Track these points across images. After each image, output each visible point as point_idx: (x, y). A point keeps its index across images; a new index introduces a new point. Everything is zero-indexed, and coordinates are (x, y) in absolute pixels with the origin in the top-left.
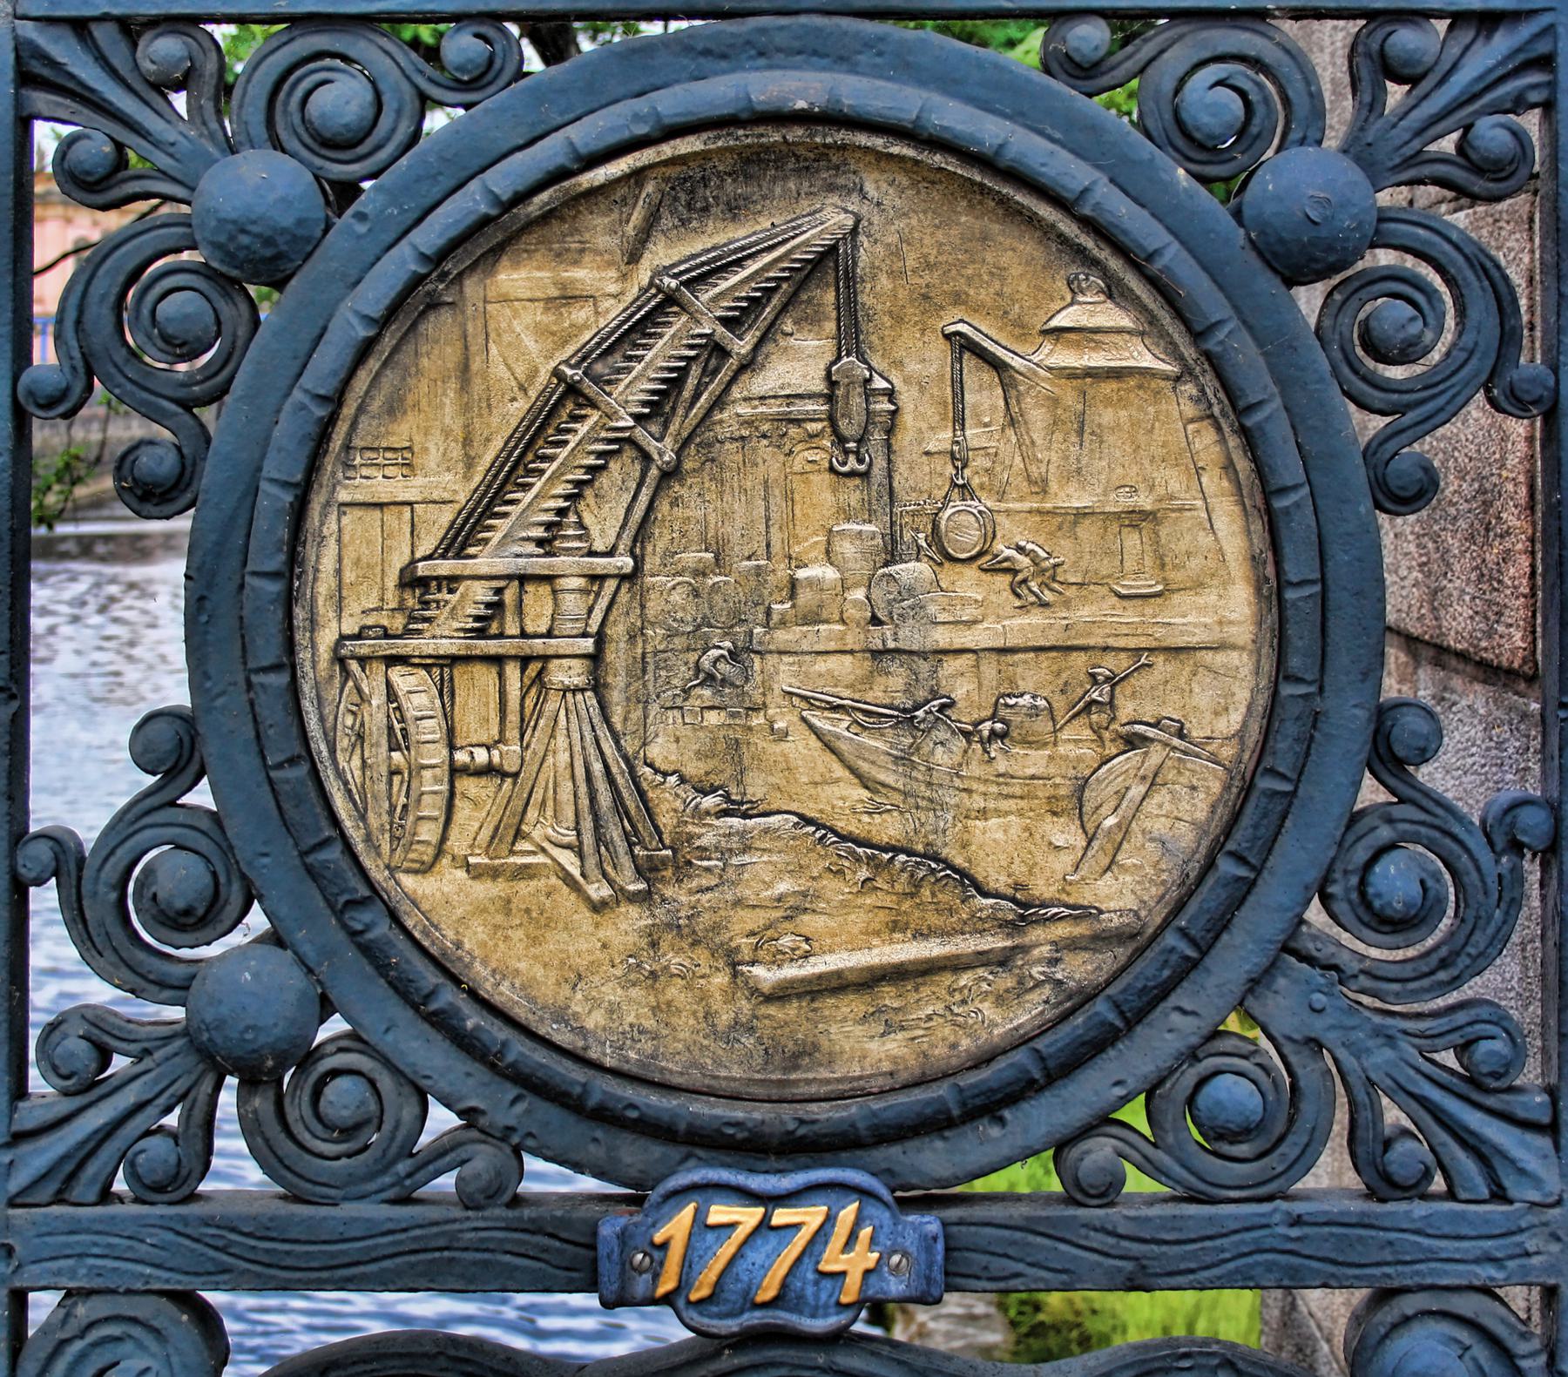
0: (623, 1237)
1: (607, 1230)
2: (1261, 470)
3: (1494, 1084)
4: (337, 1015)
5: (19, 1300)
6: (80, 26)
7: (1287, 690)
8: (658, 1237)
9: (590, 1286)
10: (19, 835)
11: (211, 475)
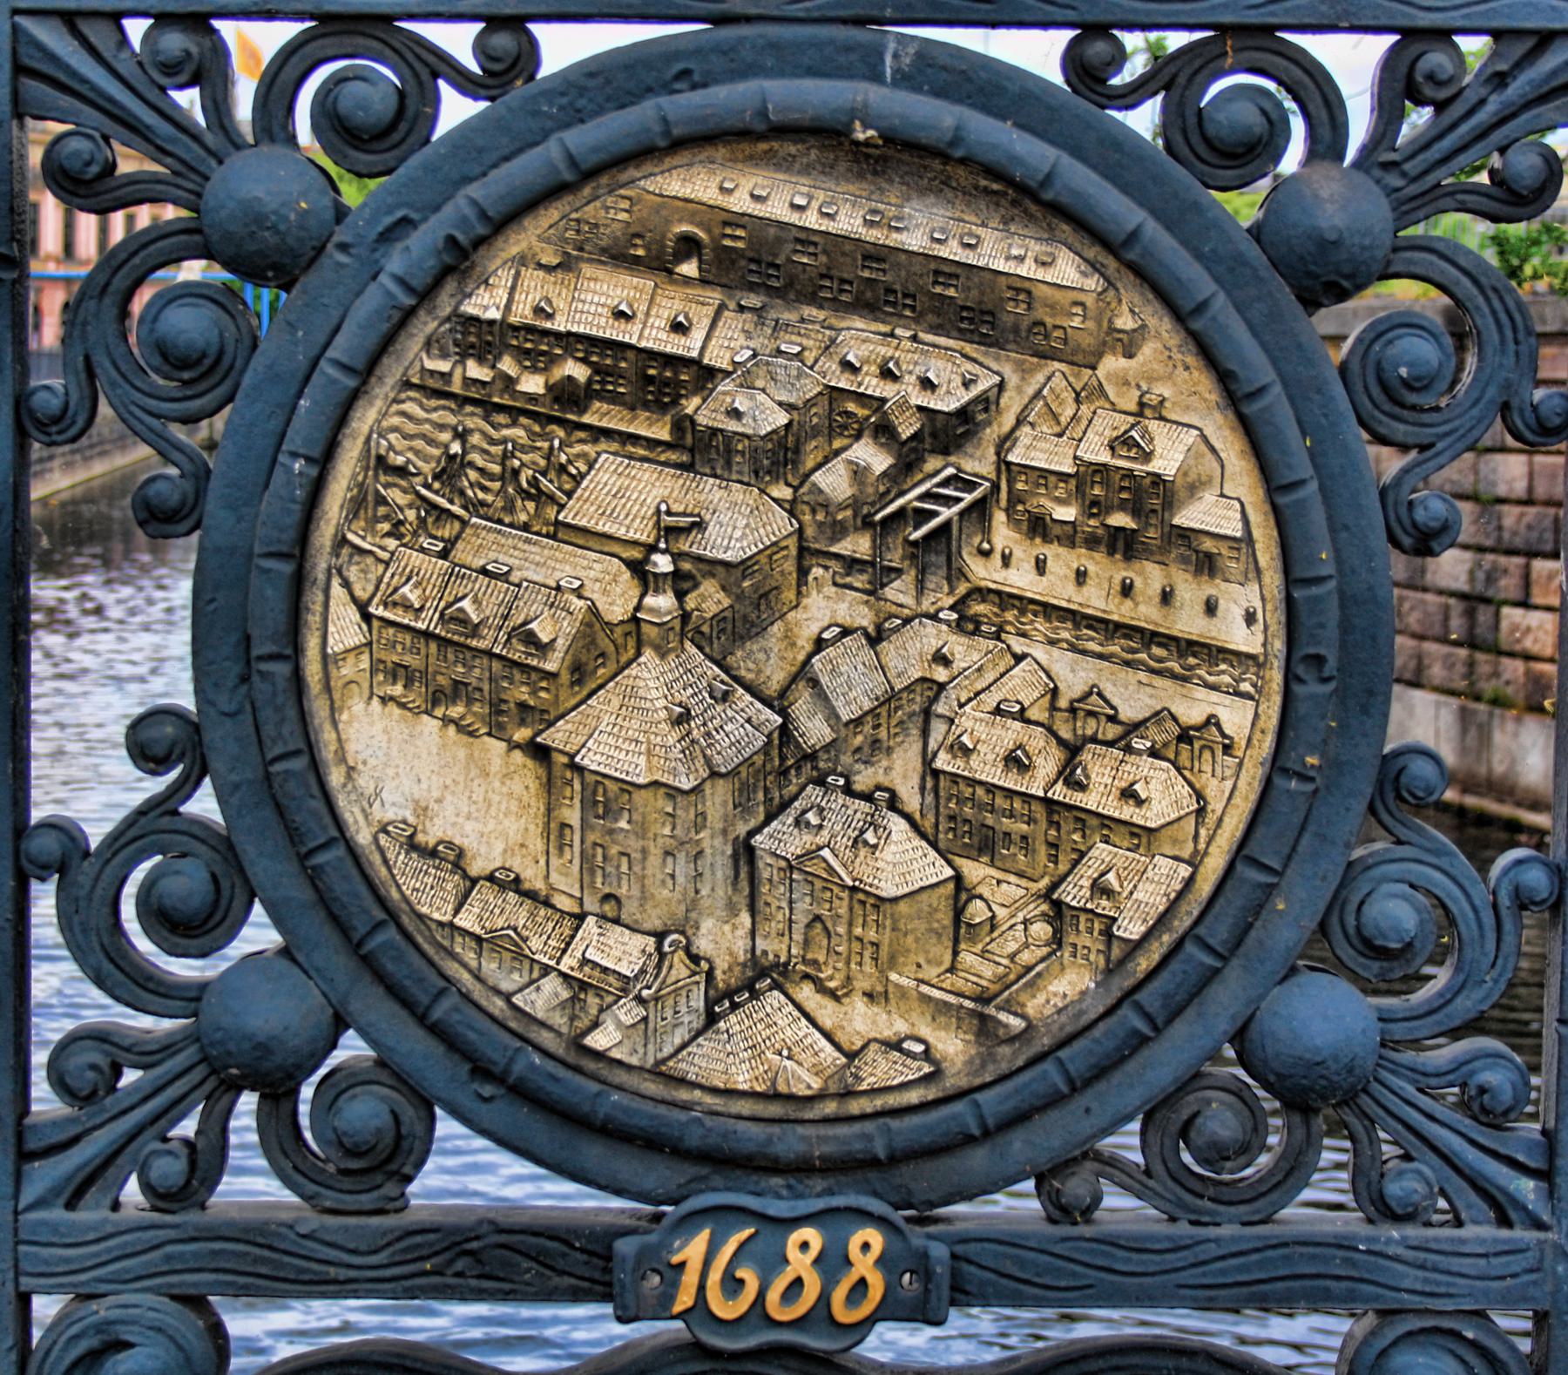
0: (643, 1254)
1: (625, 1246)
2: (1225, 378)
3: (1413, 398)
4: (351, 1032)
5: (24, 1300)
6: (69, 19)
7: (1278, 781)
8: (676, 1259)
9: (606, 1297)
10: (21, 828)
11: (213, 506)
